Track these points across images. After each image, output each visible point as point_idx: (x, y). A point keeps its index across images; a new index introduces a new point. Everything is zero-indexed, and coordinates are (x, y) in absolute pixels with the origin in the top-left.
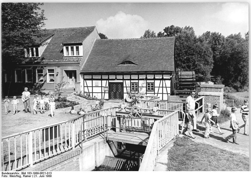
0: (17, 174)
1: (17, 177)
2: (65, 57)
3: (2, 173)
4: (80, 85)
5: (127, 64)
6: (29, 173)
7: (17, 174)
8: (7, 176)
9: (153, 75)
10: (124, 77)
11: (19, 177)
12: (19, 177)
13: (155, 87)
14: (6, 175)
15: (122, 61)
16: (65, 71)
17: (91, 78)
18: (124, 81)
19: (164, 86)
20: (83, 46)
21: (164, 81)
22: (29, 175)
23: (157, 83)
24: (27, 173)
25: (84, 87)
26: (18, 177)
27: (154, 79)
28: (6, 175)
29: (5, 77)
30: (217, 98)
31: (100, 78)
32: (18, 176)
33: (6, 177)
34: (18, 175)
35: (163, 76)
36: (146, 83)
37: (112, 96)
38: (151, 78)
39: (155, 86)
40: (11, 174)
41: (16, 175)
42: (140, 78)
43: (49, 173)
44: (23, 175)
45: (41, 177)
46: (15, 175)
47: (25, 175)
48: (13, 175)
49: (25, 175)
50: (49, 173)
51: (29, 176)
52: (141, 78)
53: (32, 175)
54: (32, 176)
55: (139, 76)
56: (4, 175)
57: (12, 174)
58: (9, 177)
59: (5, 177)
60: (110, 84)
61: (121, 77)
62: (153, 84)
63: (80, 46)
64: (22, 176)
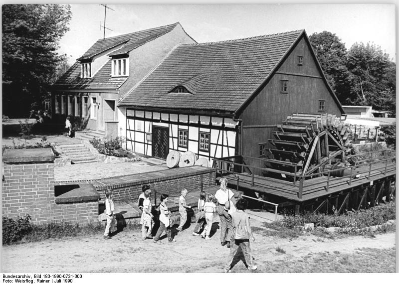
0: (27, 277)
1: (27, 283)
2: (113, 77)
3: (4, 276)
4: (117, 126)
5: (180, 92)
6: (46, 276)
7: (27, 277)
8: (11, 281)
9: (209, 117)
10: (128, 113)
11: (30, 283)
12: (30, 283)
13: (198, 141)
14: (10, 279)
15: (171, 89)
16: (106, 100)
17: (208, 124)
18: (170, 125)
19: (225, 144)
20: (130, 60)
21: (225, 132)
22: (46, 279)
23: (215, 133)
24: (42, 276)
25: (127, 130)
26: (29, 283)
27: (211, 127)
28: (10, 279)
29: (62, 108)
30: (118, 191)
31: (220, 124)
32: (29, 281)
33: (10, 283)
34: (29, 279)
35: (223, 122)
36: (199, 133)
37: (157, 152)
38: (184, 122)
39: (189, 138)
40: (18, 279)
41: (25, 279)
42: (190, 122)
43: (71, 276)
44: (36, 279)
45: (57, 283)
46: (24, 279)
47: (40, 279)
48: (21, 279)
49: (40, 279)
50: (71, 276)
51: (47, 281)
52: (193, 122)
53: (50, 279)
54: (50, 282)
55: (225, 119)
56: (7, 279)
57: (19, 277)
58: (15, 283)
59: (8, 283)
60: (154, 127)
61: (165, 117)
62: (208, 136)
63: (126, 59)
64: (35, 280)
